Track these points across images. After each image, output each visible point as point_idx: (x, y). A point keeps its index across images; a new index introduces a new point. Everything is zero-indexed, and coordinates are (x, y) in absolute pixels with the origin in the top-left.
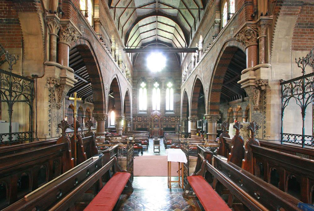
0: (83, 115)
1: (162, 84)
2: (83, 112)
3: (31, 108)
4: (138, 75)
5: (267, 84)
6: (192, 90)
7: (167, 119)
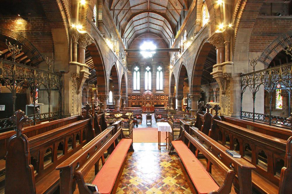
0: (87, 95)
1: (153, 68)
2: (87, 92)
3: (60, 95)
4: (133, 60)
5: (230, 76)
6: (178, 74)
7: (157, 98)
